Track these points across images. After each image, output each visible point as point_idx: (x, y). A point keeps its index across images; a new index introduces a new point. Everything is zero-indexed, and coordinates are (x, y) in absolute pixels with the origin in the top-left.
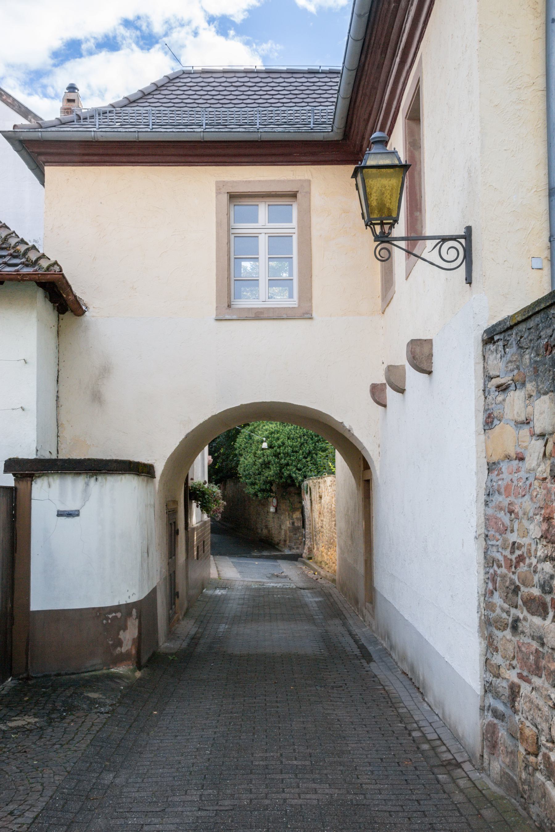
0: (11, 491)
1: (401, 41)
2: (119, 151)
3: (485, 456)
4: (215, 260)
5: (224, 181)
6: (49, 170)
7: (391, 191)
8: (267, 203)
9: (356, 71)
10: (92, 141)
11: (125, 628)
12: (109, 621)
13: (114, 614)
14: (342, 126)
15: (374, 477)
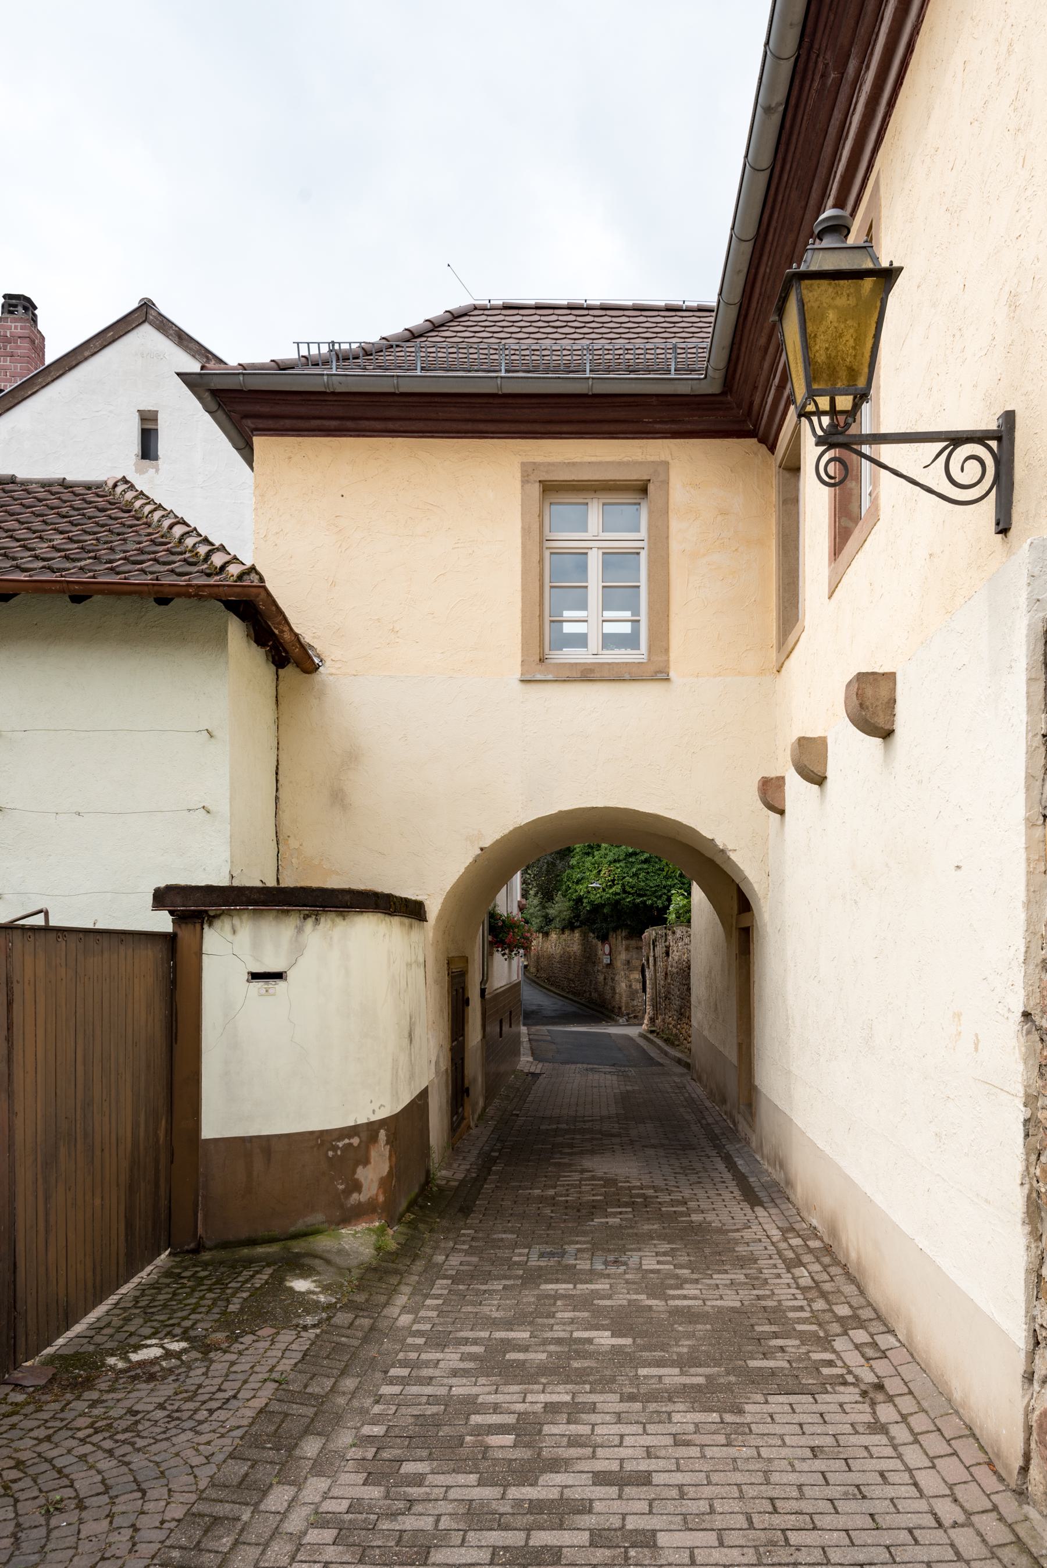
0: (169, 940)
1: (840, 160)
3: (1043, 869)
4: (519, 588)
5: (534, 463)
6: (259, 442)
7: (856, 331)
8: (602, 501)
9: (751, 243)
10: (324, 393)
11: (366, 1162)
12: (339, 1153)
13: (347, 1141)
14: (722, 365)
15: (759, 922)
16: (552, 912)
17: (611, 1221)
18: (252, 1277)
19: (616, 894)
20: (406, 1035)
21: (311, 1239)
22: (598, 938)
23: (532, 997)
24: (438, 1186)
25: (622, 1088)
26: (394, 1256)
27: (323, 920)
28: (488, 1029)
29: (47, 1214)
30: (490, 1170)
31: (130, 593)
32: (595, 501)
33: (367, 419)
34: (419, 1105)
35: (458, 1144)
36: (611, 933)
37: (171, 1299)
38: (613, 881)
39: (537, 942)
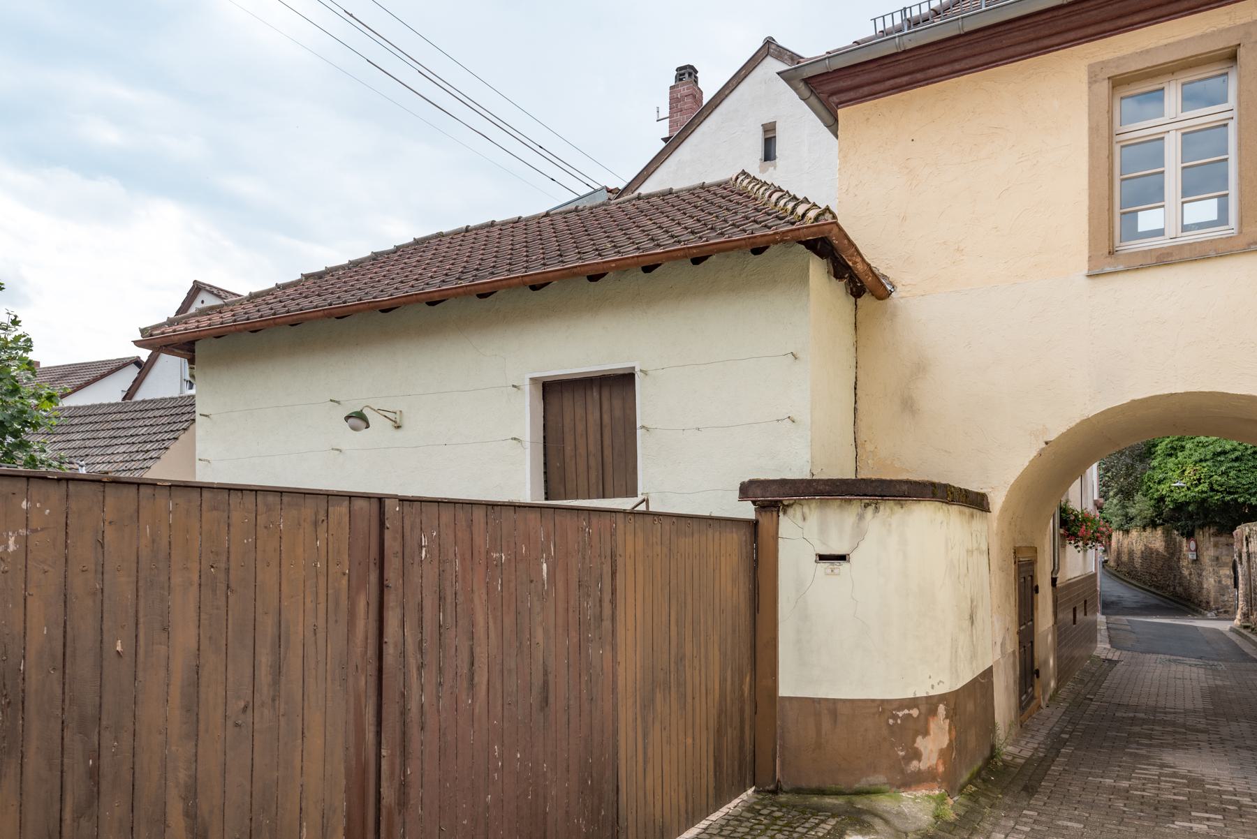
0: (754, 525)
2: (937, 60)
4: (1086, 187)
11: (926, 733)
13: (906, 711)
16: (1132, 511)
17: (1196, 826)
18: (817, 825)
19: (1203, 492)
20: (967, 617)
21: (873, 797)
22: (1182, 534)
23: (1108, 587)
24: (1003, 761)
25: (1211, 682)
26: (951, 827)
27: (882, 508)
28: (1060, 616)
29: (645, 748)
30: (1059, 751)
31: (732, 249)
32: (1173, 83)
33: (935, 66)
34: (983, 683)
35: (1027, 722)
36: (1197, 531)
37: (748, 833)
38: (1199, 480)
39: (1116, 537)
